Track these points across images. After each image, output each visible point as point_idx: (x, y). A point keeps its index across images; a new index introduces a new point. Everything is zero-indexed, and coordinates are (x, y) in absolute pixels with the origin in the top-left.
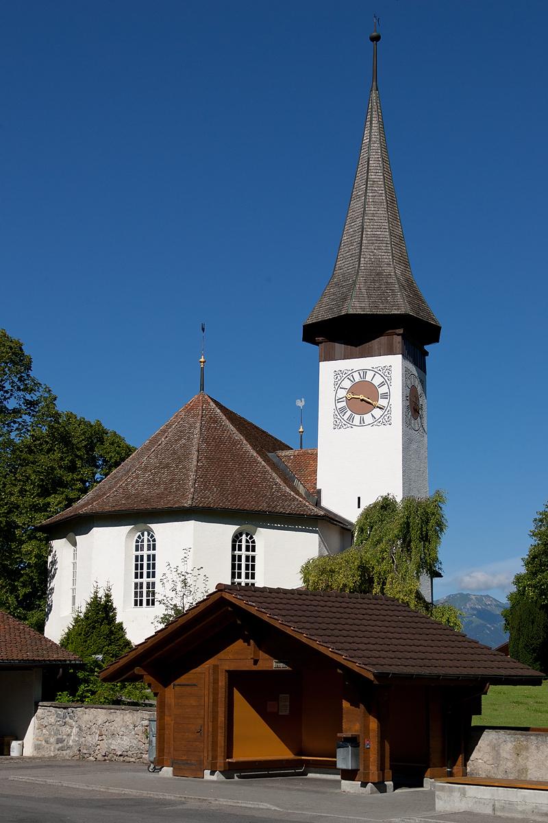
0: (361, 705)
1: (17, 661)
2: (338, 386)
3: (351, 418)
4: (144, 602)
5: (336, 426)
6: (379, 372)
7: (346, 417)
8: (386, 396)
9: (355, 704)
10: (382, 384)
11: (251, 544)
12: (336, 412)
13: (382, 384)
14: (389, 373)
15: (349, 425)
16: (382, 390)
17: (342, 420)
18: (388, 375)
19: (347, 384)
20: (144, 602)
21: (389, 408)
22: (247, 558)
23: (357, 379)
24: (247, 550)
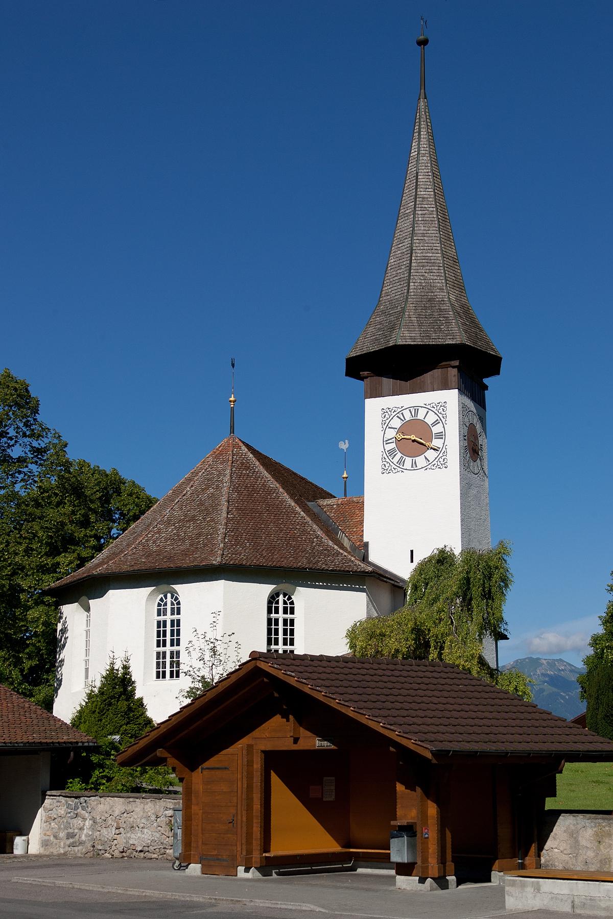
2: (386, 426)
3: (401, 462)
6: (433, 409)
8: (440, 436)
10: (436, 423)
11: (289, 606)
12: (385, 455)
13: (436, 423)
15: (399, 469)
16: (436, 429)
17: (392, 464)
21: (444, 449)
22: (285, 621)
23: (408, 417)
24: (285, 612)
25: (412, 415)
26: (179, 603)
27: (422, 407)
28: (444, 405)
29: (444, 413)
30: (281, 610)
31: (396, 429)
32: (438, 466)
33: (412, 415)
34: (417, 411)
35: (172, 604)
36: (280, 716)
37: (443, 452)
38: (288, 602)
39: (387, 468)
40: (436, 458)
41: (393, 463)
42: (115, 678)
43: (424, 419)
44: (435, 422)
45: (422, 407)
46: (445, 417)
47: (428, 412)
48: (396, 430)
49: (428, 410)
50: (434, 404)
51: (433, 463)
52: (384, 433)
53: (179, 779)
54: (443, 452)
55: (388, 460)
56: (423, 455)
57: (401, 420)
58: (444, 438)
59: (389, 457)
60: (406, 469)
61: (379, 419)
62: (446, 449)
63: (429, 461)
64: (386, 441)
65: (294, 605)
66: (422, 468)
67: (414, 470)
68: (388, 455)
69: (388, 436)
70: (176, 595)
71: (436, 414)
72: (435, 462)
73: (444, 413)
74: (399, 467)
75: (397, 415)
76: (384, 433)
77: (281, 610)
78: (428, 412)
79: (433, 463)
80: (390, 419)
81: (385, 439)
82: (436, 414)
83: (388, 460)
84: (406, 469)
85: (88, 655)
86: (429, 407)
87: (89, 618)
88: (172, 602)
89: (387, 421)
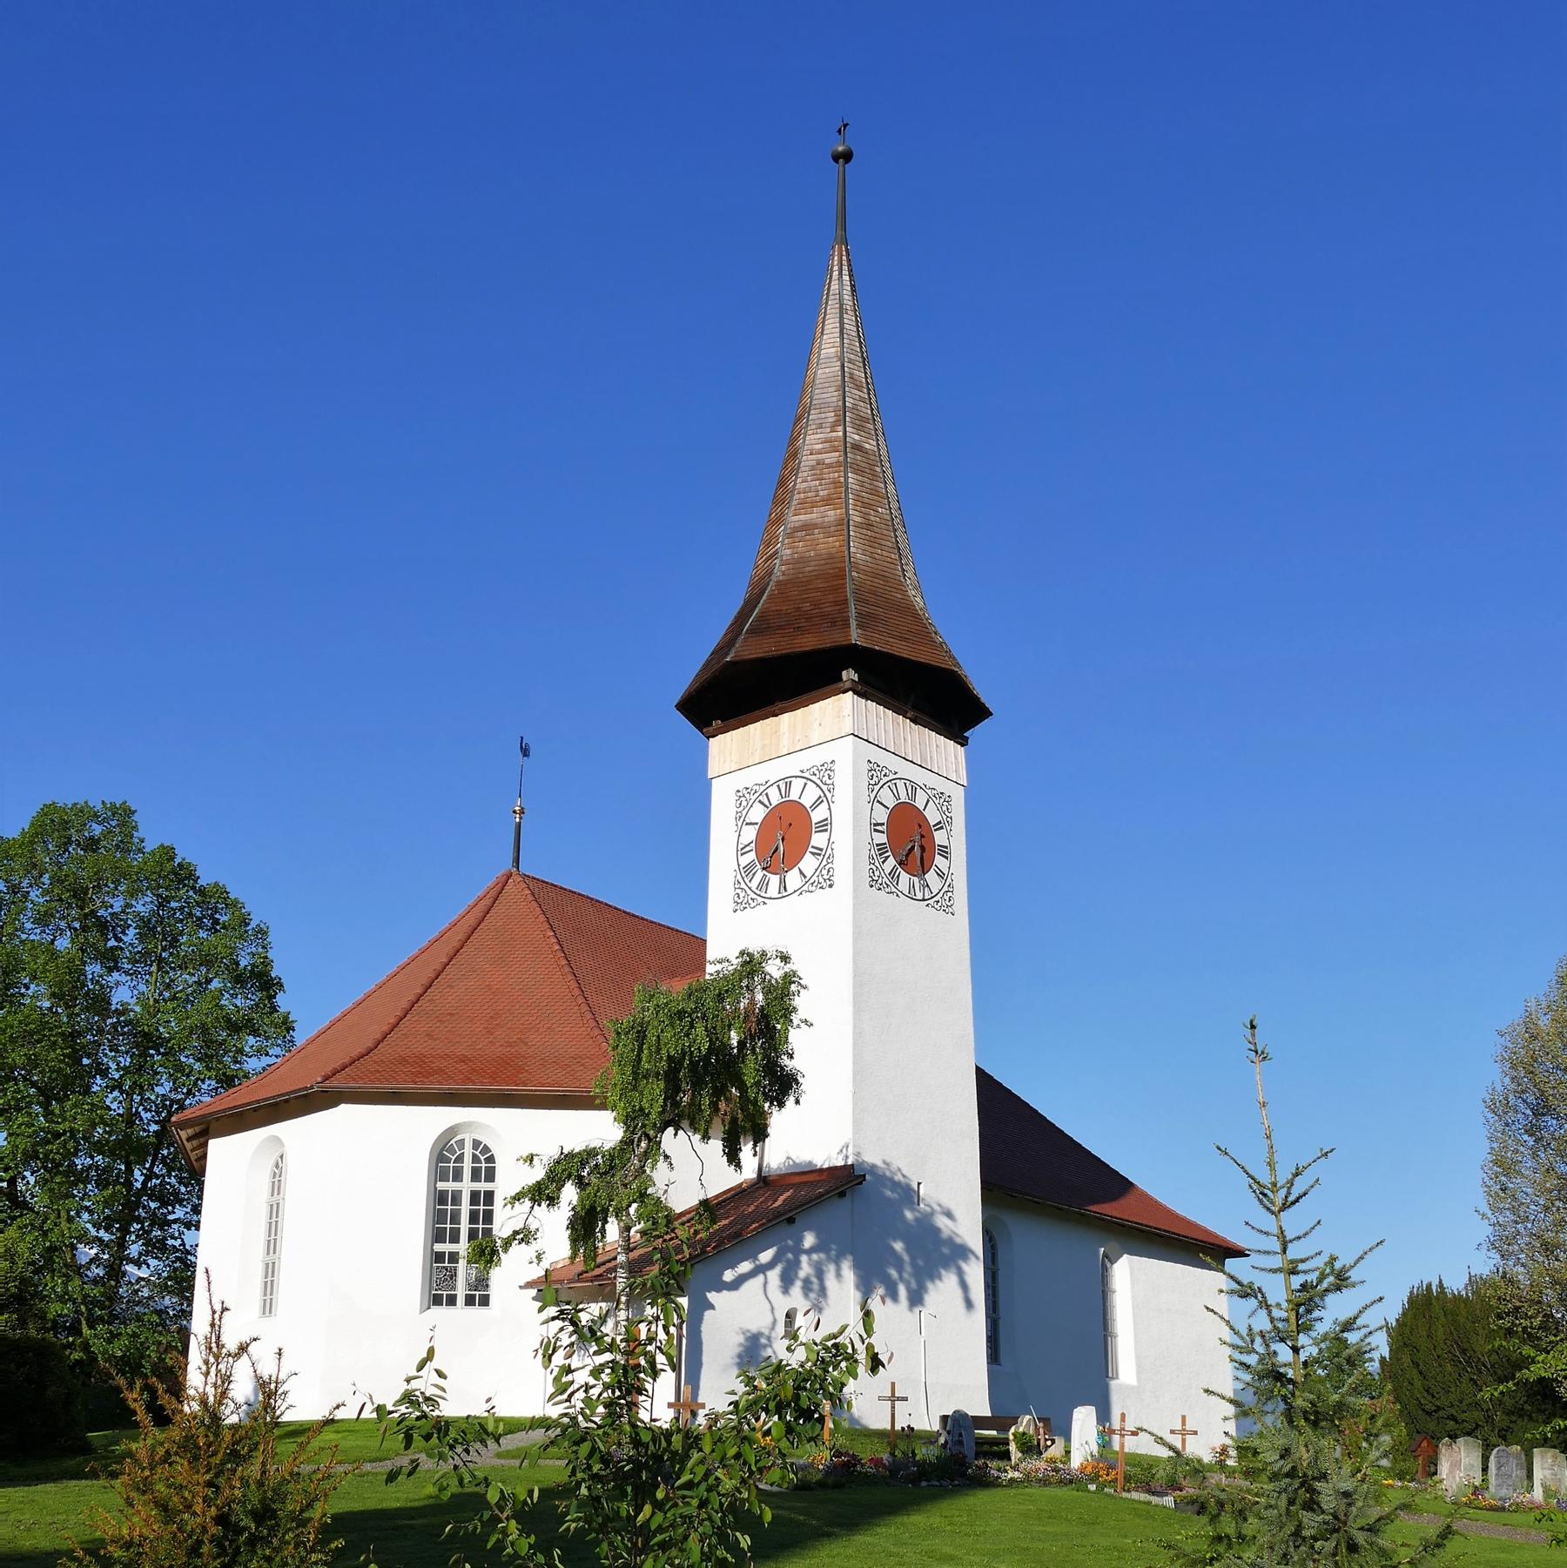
0: (709, 1295)
1: (728, 1276)
2: (742, 821)
3: (764, 884)
4: (461, 1300)
5: (740, 905)
6: (813, 778)
7: (754, 884)
8: (825, 826)
9: (710, 1292)
10: (817, 803)
11: (484, 1165)
12: (739, 877)
13: (817, 803)
14: (829, 776)
15: (760, 899)
16: (817, 816)
17: (749, 892)
18: (829, 782)
19: (758, 814)
20: (461, 1300)
21: (829, 851)
22: (475, 1196)
23: (775, 799)
24: (476, 1175)
25: (781, 794)
26: (491, 1159)
27: (796, 777)
28: (828, 768)
29: (830, 782)
30: (467, 1174)
31: (757, 824)
32: (819, 886)
33: (781, 794)
34: (789, 785)
35: (475, 1159)
36: (1456, 1283)
37: (827, 856)
38: (482, 1158)
39: (742, 899)
40: (816, 870)
41: (750, 889)
42: (69, 1300)
43: (888, 809)
44: (816, 801)
45: (796, 777)
46: (832, 790)
47: (806, 784)
48: (757, 827)
49: (805, 780)
50: (815, 769)
51: (812, 881)
52: (829, 840)
53: (1306, 1360)
54: (827, 856)
55: (743, 886)
56: (796, 868)
57: (765, 806)
58: (829, 830)
59: (745, 879)
60: (771, 898)
61: (732, 811)
62: (832, 849)
63: (805, 877)
64: (819, 855)
65: (495, 1163)
66: (795, 891)
67: (783, 897)
68: (744, 875)
69: (745, 840)
70: (452, 1142)
71: (818, 785)
72: (815, 878)
73: (830, 782)
74: (759, 895)
75: (829, 819)
76: (829, 840)
77: (467, 1174)
78: (806, 784)
79: (812, 881)
80: (749, 805)
81: (740, 846)
82: (818, 785)
83: (743, 886)
84: (771, 898)
85: (272, 1251)
86: (806, 775)
87: (277, 1178)
88: (474, 1156)
89: (744, 813)
